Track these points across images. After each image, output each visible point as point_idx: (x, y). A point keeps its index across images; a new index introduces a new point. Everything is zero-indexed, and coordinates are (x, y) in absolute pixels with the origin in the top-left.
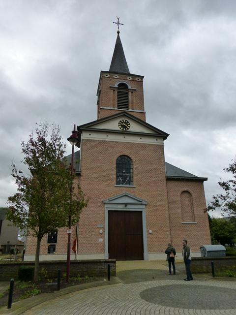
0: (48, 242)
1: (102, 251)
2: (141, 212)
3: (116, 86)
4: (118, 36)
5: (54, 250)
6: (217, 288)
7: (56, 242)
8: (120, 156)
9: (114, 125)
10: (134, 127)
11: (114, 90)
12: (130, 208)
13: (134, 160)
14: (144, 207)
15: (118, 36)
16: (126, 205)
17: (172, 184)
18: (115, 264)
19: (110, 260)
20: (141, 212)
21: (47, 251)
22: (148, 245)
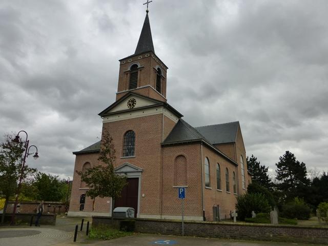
0: (81, 203)
1: (108, 211)
2: (138, 178)
3: (129, 69)
4: (147, 16)
5: (83, 209)
6: (15, 231)
7: (84, 203)
8: (125, 134)
9: (124, 106)
10: (140, 103)
11: (127, 74)
12: (130, 176)
13: (136, 133)
14: (140, 174)
15: (147, 16)
16: (126, 173)
17: (167, 150)
18: (55, 219)
19: (279, 225)
20: (138, 178)
21: (79, 209)
22: (141, 207)
